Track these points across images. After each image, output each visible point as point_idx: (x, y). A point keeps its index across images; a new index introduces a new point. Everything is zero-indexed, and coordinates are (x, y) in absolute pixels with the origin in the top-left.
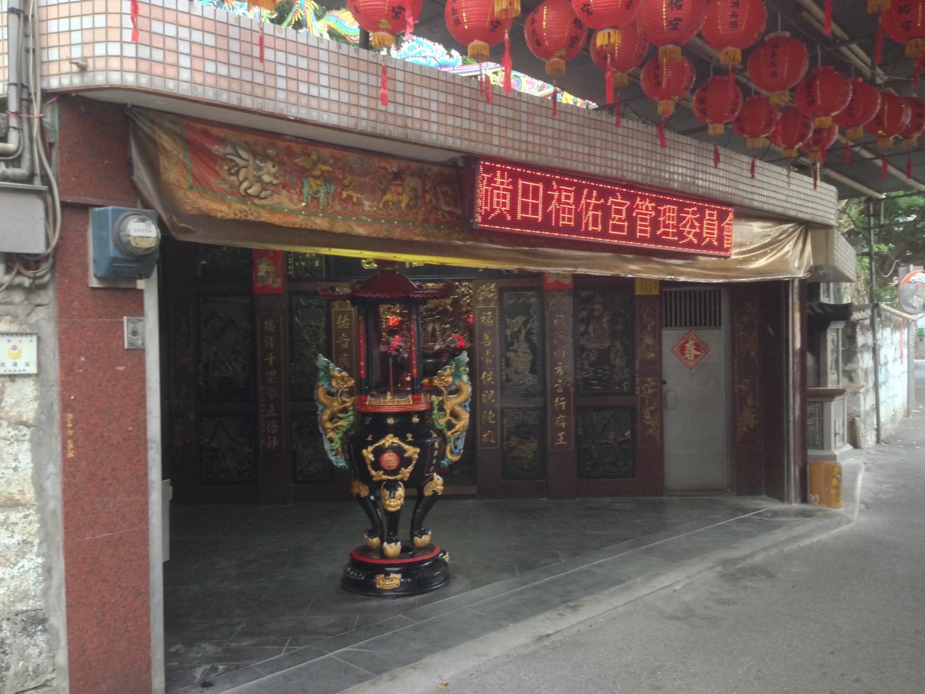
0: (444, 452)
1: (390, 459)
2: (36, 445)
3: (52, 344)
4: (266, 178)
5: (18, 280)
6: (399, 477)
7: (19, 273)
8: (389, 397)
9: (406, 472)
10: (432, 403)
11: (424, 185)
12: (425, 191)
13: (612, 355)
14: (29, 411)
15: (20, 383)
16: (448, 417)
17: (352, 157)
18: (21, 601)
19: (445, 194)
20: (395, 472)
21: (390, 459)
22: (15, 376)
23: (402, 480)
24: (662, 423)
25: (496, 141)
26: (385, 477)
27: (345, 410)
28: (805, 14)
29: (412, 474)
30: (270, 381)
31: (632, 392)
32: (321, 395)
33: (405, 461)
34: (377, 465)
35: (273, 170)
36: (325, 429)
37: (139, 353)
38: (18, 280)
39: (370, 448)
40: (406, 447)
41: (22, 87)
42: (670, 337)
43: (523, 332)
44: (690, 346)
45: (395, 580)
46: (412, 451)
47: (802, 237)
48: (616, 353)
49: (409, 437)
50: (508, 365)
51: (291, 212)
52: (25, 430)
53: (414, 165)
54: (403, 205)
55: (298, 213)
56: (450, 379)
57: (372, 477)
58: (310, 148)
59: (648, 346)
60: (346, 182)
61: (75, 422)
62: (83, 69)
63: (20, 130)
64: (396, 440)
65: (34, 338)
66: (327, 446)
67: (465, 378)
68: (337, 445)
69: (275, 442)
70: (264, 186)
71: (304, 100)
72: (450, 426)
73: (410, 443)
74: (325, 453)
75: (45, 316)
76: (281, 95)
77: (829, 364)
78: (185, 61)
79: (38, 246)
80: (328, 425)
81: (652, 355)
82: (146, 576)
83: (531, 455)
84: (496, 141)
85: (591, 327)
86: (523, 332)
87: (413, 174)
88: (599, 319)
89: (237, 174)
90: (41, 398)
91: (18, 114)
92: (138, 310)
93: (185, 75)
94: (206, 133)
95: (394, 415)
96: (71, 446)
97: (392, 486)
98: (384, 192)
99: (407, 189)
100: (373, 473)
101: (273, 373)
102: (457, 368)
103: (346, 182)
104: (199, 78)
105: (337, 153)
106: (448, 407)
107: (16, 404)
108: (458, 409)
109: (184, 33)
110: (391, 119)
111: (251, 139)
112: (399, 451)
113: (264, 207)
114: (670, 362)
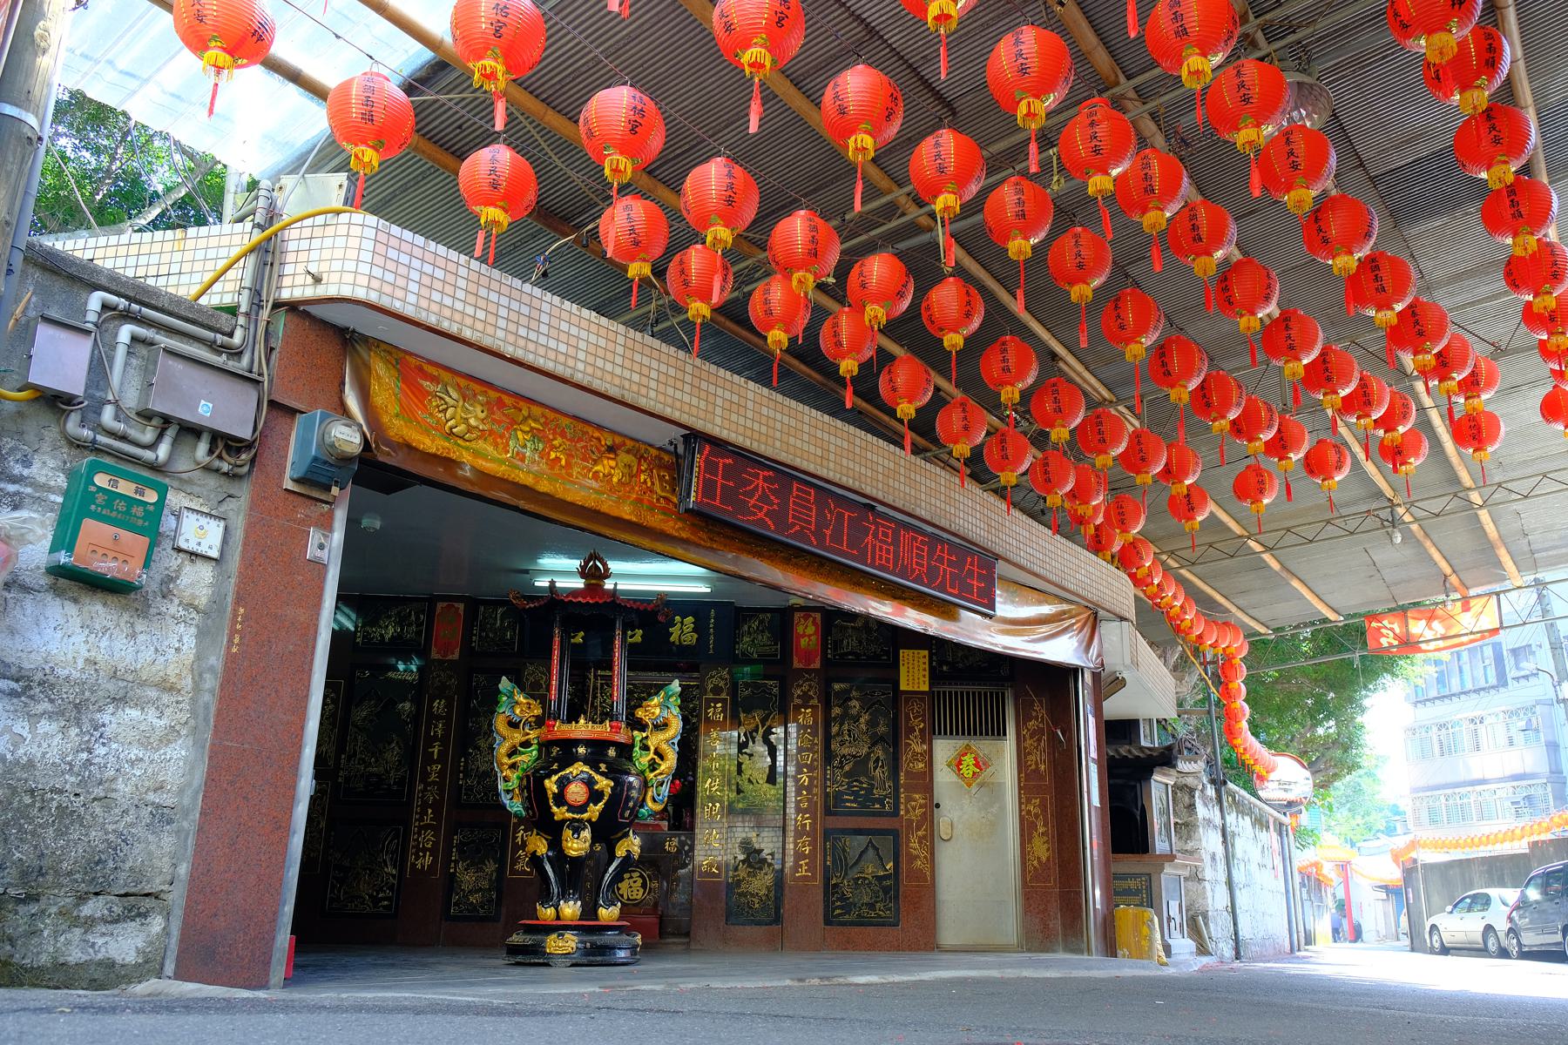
0: (644, 800)
1: (576, 792)
2: (201, 634)
3: (238, 535)
4: (472, 422)
5: (217, 463)
6: (585, 816)
7: (220, 457)
8: (582, 721)
9: (594, 811)
10: (633, 738)
11: (639, 464)
12: (640, 471)
13: (871, 765)
14: (203, 597)
15: (199, 563)
16: (652, 755)
17: (565, 422)
18: (155, 791)
19: (661, 478)
20: (582, 809)
21: (576, 792)
22: (197, 555)
23: (589, 821)
24: (932, 854)
25: (718, 420)
26: (569, 815)
27: (526, 744)
28: (1061, 364)
29: (602, 814)
30: (433, 777)
31: (896, 813)
32: (500, 724)
33: (595, 796)
34: (560, 799)
35: (482, 416)
36: (501, 765)
37: (322, 568)
38: (217, 463)
39: (555, 778)
40: (597, 777)
41: (256, 293)
42: (944, 749)
43: (761, 731)
44: (969, 760)
45: (568, 943)
46: (604, 784)
47: (1089, 624)
48: (877, 760)
49: (603, 767)
50: (740, 772)
51: (493, 460)
52: (194, 615)
53: (629, 444)
54: (615, 480)
55: (502, 462)
56: (657, 711)
57: (553, 814)
58: (522, 404)
59: (915, 754)
60: (556, 443)
61: (246, 617)
62: (317, 280)
63: (246, 329)
64: (586, 769)
65: (222, 524)
66: (501, 786)
67: (676, 711)
68: (514, 783)
69: (428, 860)
70: (470, 429)
71: (522, 342)
72: (653, 766)
73: (602, 774)
74: (498, 795)
75: (238, 509)
76: (500, 334)
77: (1156, 827)
78: (413, 287)
79: (245, 433)
80: (505, 760)
81: (921, 765)
82: (289, 810)
83: (764, 891)
84: (718, 420)
85: (846, 727)
86: (761, 731)
87: (628, 452)
88: (856, 719)
89: (445, 411)
90: (217, 585)
91: (247, 314)
92: (326, 525)
93: (412, 298)
94: (420, 369)
95: (587, 743)
96: (236, 640)
97: (577, 828)
98: (595, 462)
99: (621, 465)
100: (555, 809)
101: (427, 820)
102: (668, 697)
103: (556, 443)
104: (424, 303)
105: (551, 415)
106: (652, 743)
107: (192, 585)
108: (664, 746)
109: (416, 263)
110: (608, 378)
111: (463, 382)
112: (590, 783)
113: (467, 449)
114: (943, 777)
